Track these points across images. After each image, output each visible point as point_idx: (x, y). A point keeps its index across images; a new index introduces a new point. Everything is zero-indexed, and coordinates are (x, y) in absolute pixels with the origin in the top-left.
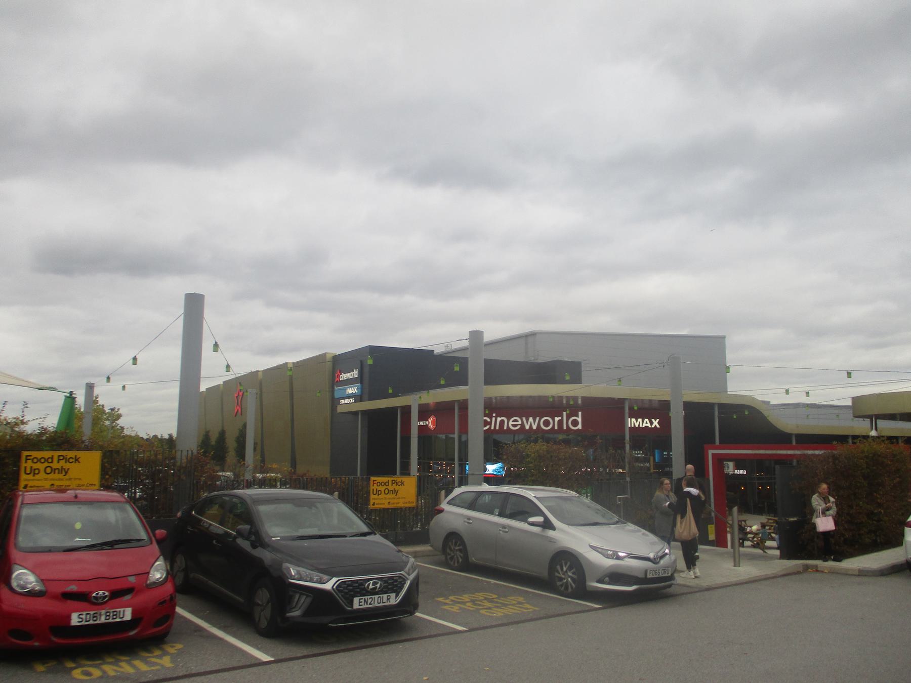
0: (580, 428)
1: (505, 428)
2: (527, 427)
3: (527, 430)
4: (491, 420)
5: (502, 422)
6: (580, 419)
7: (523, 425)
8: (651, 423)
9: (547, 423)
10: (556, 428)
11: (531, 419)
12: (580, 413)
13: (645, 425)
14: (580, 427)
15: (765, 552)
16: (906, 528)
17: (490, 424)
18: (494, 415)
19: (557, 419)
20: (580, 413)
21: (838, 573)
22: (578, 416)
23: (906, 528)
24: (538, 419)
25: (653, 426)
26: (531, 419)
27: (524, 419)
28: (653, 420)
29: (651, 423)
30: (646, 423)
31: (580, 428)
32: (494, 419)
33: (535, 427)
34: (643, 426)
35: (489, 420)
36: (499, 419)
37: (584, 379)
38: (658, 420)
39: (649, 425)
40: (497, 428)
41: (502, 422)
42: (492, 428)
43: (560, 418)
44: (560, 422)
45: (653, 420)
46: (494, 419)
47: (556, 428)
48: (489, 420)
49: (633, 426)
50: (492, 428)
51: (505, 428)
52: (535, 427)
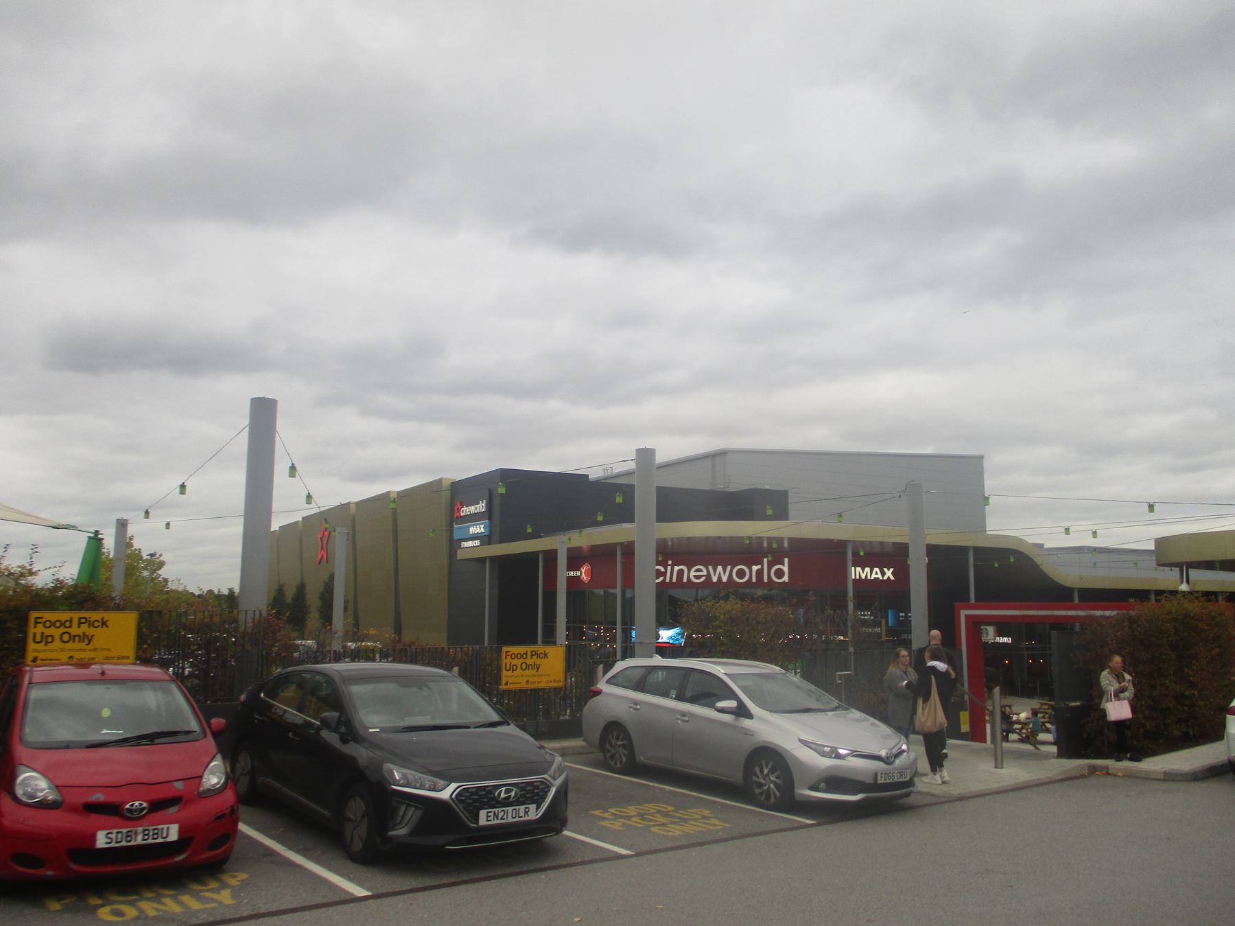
0: (787, 581)
1: (685, 580)
2: (715, 579)
3: (715, 583)
4: (666, 569)
5: (681, 572)
6: (786, 569)
7: (708, 576)
8: (883, 574)
9: (741, 574)
10: (754, 580)
11: (720, 568)
12: (786, 560)
13: (874, 576)
14: (786, 578)
15: (1036, 748)
16: (1228, 715)
17: (664, 574)
18: (670, 562)
19: (755, 568)
20: (786, 560)
21: (1136, 777)
22: (783, 564)
23: (1228, 715)
24: (729, 568)
25: (885, 578)
26: (720, 568)
27: (710, 568)
28: (885, 569)
29: (883, 574)
30: (876, 573)
31: (787, 581)
32: (669, 568)
33: (725, 579)
34: (872, 578)
35: (662, 569)
36: (676, 568)
37: (791, 513)
38: (892, 570)
39: (879, 576)
40: (674, 580)
41: (681, 572)
42: (668, 580)
43: (759, 567)
44: (760, 572)
45: (885, 569)
46: (669, 568)
47: (754, 580)
48: (662, 569)
49: (858, 577)
50: (668, 580)
51: (685, 580)
52: (725, 579)
